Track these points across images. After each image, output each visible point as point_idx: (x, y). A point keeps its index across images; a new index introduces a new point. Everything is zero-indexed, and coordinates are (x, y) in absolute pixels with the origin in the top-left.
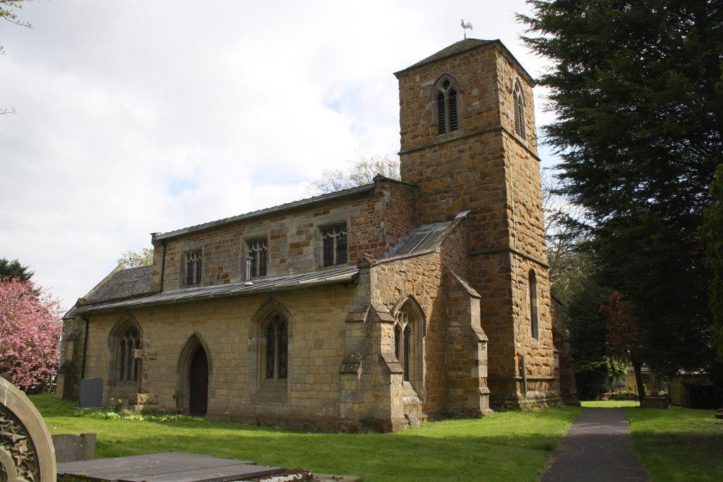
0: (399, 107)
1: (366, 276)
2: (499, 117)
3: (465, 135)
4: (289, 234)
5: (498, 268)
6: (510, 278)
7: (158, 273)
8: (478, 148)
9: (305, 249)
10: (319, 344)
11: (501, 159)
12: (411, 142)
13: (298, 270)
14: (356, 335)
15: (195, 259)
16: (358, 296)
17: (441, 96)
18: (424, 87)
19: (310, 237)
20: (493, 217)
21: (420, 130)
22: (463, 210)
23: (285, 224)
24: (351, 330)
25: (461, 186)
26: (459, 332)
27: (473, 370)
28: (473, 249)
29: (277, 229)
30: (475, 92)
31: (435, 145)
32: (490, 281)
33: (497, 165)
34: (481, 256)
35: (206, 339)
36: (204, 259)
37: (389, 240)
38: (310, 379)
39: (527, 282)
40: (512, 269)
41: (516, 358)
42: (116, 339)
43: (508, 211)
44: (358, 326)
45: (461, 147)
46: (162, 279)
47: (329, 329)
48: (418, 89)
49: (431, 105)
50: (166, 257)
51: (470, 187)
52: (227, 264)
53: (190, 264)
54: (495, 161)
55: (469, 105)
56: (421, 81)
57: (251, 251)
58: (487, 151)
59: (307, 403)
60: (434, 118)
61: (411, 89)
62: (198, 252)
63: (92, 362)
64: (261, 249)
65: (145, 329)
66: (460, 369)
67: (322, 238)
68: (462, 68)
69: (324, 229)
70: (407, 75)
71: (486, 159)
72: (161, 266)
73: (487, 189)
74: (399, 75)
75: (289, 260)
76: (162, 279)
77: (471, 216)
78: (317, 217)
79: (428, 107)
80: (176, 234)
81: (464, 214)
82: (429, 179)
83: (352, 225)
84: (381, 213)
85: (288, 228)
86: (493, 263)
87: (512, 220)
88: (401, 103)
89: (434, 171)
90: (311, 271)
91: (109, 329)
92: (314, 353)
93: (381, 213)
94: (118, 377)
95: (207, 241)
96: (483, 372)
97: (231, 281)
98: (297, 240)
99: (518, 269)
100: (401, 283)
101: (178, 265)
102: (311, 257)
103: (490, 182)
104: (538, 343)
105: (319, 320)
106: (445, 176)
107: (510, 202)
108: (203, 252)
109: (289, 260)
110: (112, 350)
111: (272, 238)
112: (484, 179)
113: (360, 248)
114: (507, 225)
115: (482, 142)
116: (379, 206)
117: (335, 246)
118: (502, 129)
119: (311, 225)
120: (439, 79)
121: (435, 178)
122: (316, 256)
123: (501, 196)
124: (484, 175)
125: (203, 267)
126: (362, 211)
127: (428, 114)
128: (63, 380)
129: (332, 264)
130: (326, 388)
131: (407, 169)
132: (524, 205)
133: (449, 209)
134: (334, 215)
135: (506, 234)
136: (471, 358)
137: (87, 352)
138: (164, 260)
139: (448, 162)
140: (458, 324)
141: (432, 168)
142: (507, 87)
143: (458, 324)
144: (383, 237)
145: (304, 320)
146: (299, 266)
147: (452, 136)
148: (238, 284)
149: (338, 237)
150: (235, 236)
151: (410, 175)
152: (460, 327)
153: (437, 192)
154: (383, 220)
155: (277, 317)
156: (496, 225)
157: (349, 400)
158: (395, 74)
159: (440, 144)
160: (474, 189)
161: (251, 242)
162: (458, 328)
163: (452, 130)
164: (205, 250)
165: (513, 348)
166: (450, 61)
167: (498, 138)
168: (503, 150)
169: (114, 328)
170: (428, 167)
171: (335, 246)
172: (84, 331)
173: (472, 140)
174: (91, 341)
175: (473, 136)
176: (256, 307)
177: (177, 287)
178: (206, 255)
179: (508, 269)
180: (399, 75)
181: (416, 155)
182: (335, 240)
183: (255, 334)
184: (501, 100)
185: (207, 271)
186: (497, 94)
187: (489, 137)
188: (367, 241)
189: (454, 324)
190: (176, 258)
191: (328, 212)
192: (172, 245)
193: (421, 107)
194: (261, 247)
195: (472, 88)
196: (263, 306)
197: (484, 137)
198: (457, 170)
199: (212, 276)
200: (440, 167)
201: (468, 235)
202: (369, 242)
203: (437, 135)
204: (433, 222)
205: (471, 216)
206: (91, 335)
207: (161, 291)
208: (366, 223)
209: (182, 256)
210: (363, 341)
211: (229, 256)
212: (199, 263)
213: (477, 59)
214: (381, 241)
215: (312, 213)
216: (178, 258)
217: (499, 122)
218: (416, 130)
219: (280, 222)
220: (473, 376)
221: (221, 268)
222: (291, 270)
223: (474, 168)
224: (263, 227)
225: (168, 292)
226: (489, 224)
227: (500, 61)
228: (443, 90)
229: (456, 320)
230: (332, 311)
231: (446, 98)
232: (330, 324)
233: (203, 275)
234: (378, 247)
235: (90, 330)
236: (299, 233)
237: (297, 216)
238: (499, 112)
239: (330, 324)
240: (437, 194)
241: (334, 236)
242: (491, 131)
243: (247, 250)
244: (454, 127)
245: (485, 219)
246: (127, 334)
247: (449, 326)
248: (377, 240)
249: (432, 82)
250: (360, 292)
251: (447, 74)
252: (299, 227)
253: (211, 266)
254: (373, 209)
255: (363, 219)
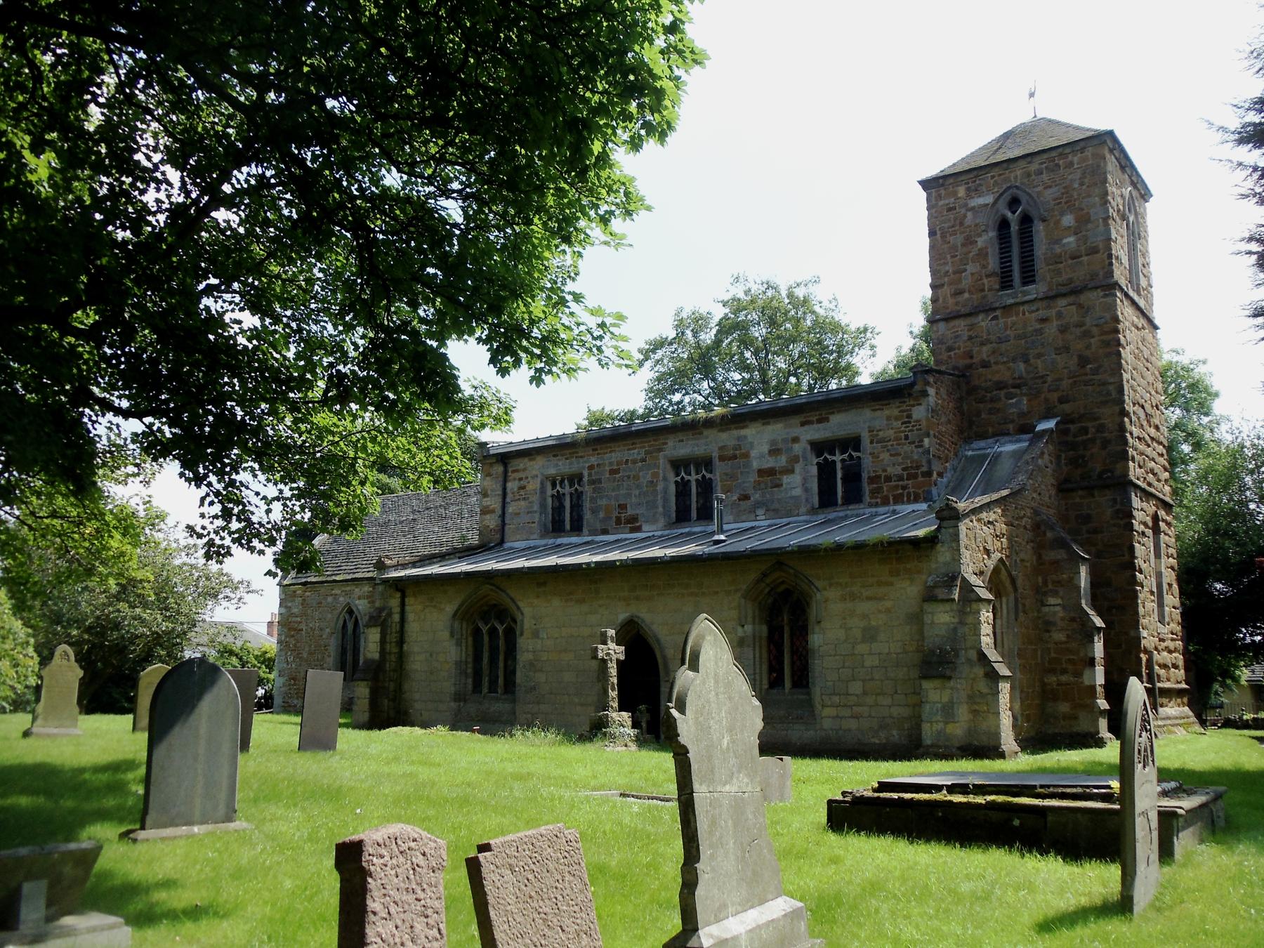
0: (927, 240)
1: (951, 530)
2: (1111, 264)
3: (1051, 294)
4: (754, 453)
5: (1109, 512)
6: (1131, 528)
7: (493, 511)
8: (1072, 315)
9: (786, 479)
10: (870, 635)
11: (1111, 336)
12: (951, 301)
13: (774, 512)
14: (942, 620)
15: (567, 489)
16: (937, 562)
17: (1004, 225)
18: (973, 209)
19: (795, 459)
20: (1101, 428)
21: (966, 281)
22: (1047, 417)
23: (745, 437)
24: (932, 613)
25: (1042, 377)
26: (1061, 615)
27: (1087, 673)
28: (1066, 481)
29: (732, 443)
30: (1068, 220)
31: (995, 309)
32: (1095, 531)
33: (1107, 344)
34: (1080, 493)
35: (654, 627)
36: (587, 489)
37: (937, 467)
38: (856, 688)
39: (1149, 532)
40: (1135, 513)
41: (1144, 657)
42: (464, 625)
43: (1126, 419)
44: (947, 606)
45: (1042, 313)
46: (503, 521)
47: (888, 611)
48: (963, 211)
49: (987, 239)
50: (509, 485)
51: (1060, 379)
52: (634, 500)
53: (559, 498)
54: (1104, 337)
55: (1058, 241)
56: (969, 196)
57: (678, 479)
58: (1088, 320)
59: (852, 724)
60: (993, 263)
61: (950, 210)
62: (575, 479)
63: (417, 663)
64: (699, 477)
65: (527, 610)
66: (1064, 671)
67: (815, 461)
68: (1045, 177)
69: (819, 447)
70: (943, 185)
71: (1087, 334)
72: (500, 499)
73: (1086, 383)
74: (926, 184)
75: (756, 496)
76: (503, 521)
77: (1061, 427)
78: (806, 427)
79: (981, 242)
80: (531, 446)
81: (1050, 424)
82: (985, 365)
83: (872, 442)
84: (924, 423)
85: (752, 444)
86: (1102, 503)
87: (1131, 434)
88: (932, 234)
89: (994, 352)
90: (798, 515)
91: (450, 608)
92: (862, 648)
93: (924, 423)
94: (470, 687)
95: (594, 460)
96: (1100, 679)
97: (645, 528)
98: (770, 463)
99: (1142, 511)
100: (989, 539)
101: (535, 498)
102: (798, 492)
103: (1095, 372)
104: (1164, 630)
105: (869, 598)
106: (1014, 360)
107: (1129, 407)
108: (586, 479)
109: (756, 496)
110: (458, 644)
111: (722, 458)
112: (1084, 367)
113: (888, 479)
114: (1126, 443)
115: (1080, 306)
116: (919, 412)
117: (839, 475)
118: (1116, 285)
119: (796, 440)
120: (1002, 194)
121: (996, 363)
122: (806, 490)
123: (1114, 394)
124: (1083, 361)
125: (587, 505)
126: (889, 418)
127: (982, 254)
128: (367, 691)
129: (836, 504)
130: (886, 701)
131: (944, 347)
132: (1143, 407)
133: (1022, 415)
134: (838, 424)
135: (1124, 457)
136: (1082, 654)
137: (405, 647)
138: (504, 489)
139: (1018, 337)
140: (1059, 601)
141: (989, 346)
142: (1119, 210)
143: (1059, 601)
144: (929, 462)
145: (843, 599)
146: (776, 506)
147: (1025, 293)
148: (659, 533)
149: (843, 461)
150: (647, 453)
151: (950, 357)
152: (1064, 607)
153: (1000, 386)
154: (928, 435)
155: (788, 593)
156: (1106, 443)
157: (939, 718)
158: (921, 182)
159: (1004, 307)
160: (1065, 383)
161: (678, 465)
162: (1058, 608)
163: (1025, 283)
164: (590, 475)
165: (1138, 639)
166: (1022, 163)
167: (1109, 300)
168: (1117, 321)
169: (461, 606)
170: (982, 344)
171: (839, 475)
172: (397, 610)
173: (1062, 302)
174: (413, 627)
175: (1064, 295)
176: (752, 576)
177: (535, 536)
178: (592, 482)
179: (1127, 514)
180: (926, 184)
181: (961, 324)
182: (839, 466)
183: (750, 619)
184: (1114, 235)
185: (594, 511)
186: (1107, 225)
187: (1093, 298)
188: (899, 468)
189: (1052, 601)
190: (530, 487)
191: (827, 420)
192: (521, 463)
193: (969, 242)
194: (677, 475)
195: (1062, 214)
196: (765, 575)
197: (1083, 298)
198: (1036, 351)
199: (607, 518)
200: (1003, 347)
201: (1058, 457)
202: (904, 469)
203: (998, 290)
204: (994, 435)
205: (1061, 427)
206: (410, 617)
207: (502, 542)
208: (897, 439)
209: (542, 483)
210: (955, 629)
211: (638, 487)
212: (579, 495)
213: (1071, 164)
214: (924, 469)
215: (796, 420)
216: (533, 485)
217: (1111, 273)
218: (960, 281)
219: (735, 433)
220: (1087, 683)
221: (623, 507)
222: (760, 512)
223: (1066, 349)
224: (703, 441)
225: (517, 545)
226: (1093, 440)
227: (1111, 164)
228: (1009, 214)
229: (1055, 594)
230: (892, 584)
231: (1014, 228)
232: (888, 604)
233: (587, 516)
234: (920, 479)
235: (408, 608)
236: (774, 452)
237: (768, 423)
238: (1110, 256)
239: (888, 604)
240: (1000, 389)
241: (838, 458)
242: (1097, 288)
243: (672, 478)
244: (1029, 277)
245: (1087, 433)
246: (485, 617)
247: (1043, 605)
248: (918, 467)
249: (989, 199)
250: (942, 554)
251: (1017, 187)
252: (773, 442)
253: (604, 502)
254: (909, 416)
255: (892, 432)
